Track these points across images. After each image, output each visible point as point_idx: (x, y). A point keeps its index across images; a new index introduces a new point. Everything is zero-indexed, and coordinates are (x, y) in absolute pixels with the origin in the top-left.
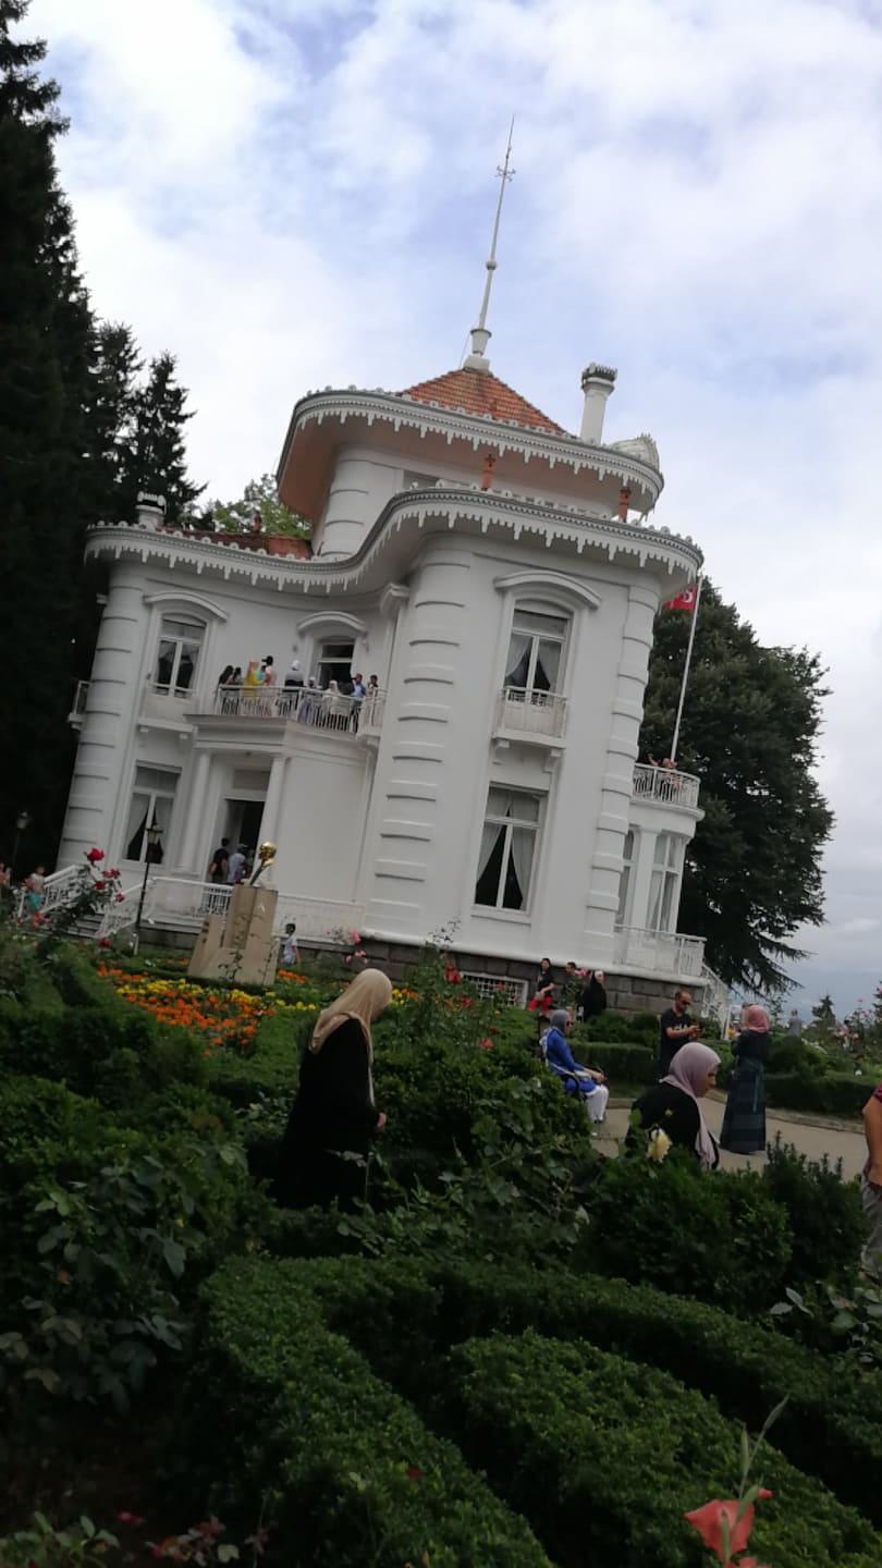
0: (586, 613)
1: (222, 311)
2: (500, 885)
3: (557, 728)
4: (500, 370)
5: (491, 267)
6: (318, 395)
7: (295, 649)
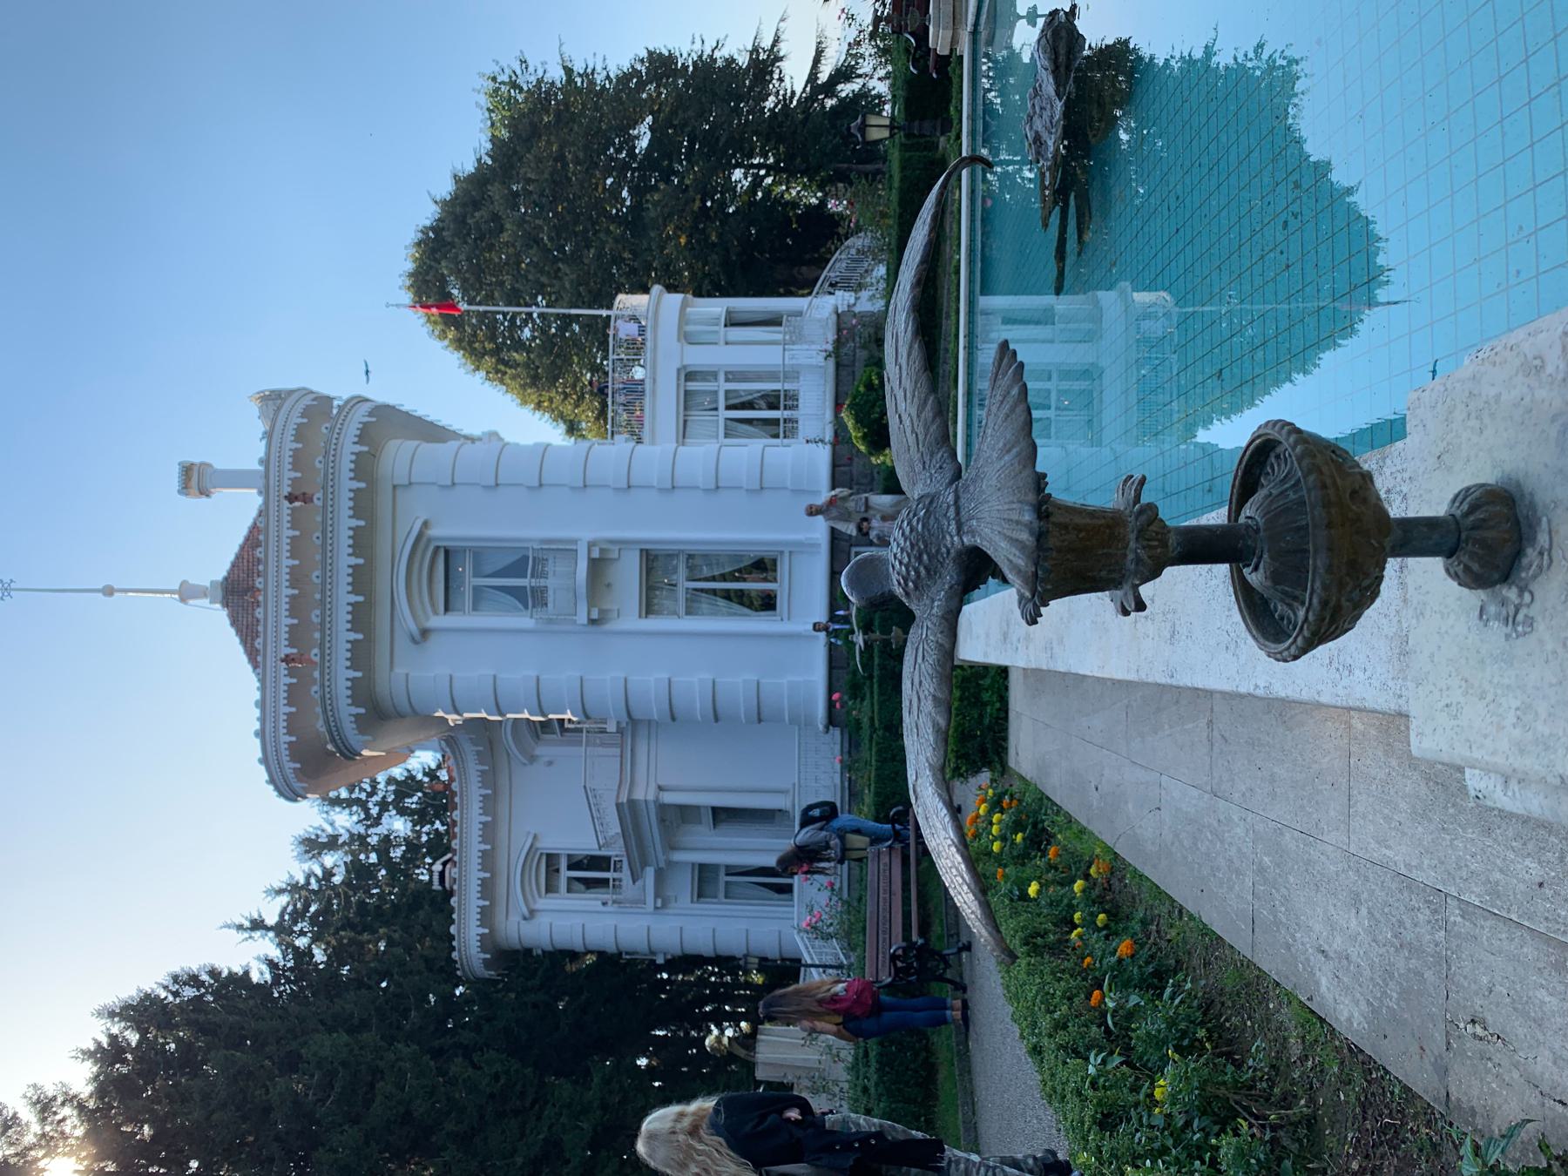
0: (433, 532)
1: (214, 872)
2: (748, 582)
3: (567, 551)
4: (220, 571)
5: (109, 591)
6: (277, 788)
7: (550, 763)
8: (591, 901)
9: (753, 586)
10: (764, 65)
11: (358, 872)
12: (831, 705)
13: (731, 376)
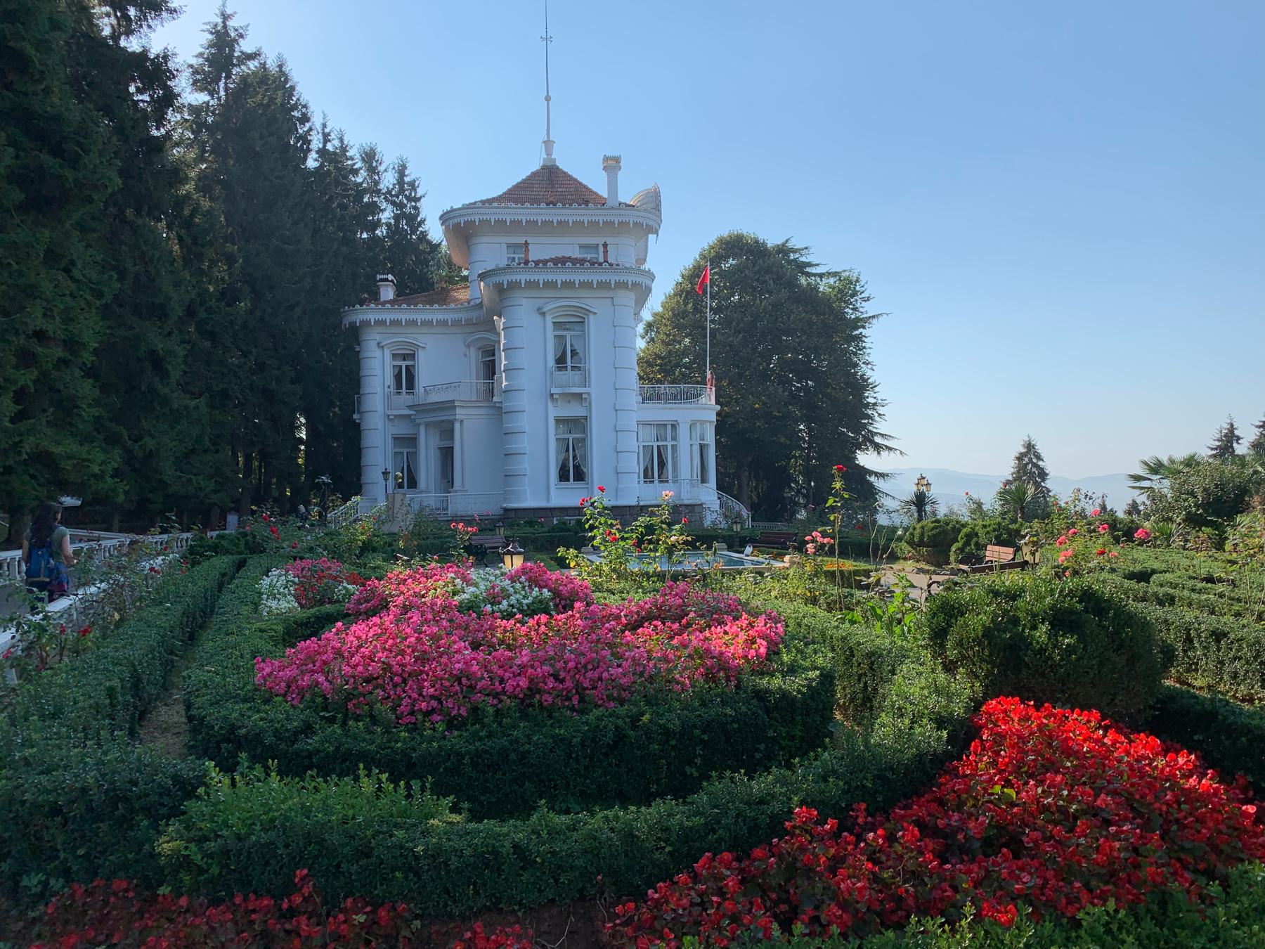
0: (591, 316)
2: (572, 471)
3: (584, 384)
4: (562, 165)
5: (548, 99)
6: (448, 212)
8: (390, 380)
10: (870, 441)
11: (360, 193)
12: (516, 510)
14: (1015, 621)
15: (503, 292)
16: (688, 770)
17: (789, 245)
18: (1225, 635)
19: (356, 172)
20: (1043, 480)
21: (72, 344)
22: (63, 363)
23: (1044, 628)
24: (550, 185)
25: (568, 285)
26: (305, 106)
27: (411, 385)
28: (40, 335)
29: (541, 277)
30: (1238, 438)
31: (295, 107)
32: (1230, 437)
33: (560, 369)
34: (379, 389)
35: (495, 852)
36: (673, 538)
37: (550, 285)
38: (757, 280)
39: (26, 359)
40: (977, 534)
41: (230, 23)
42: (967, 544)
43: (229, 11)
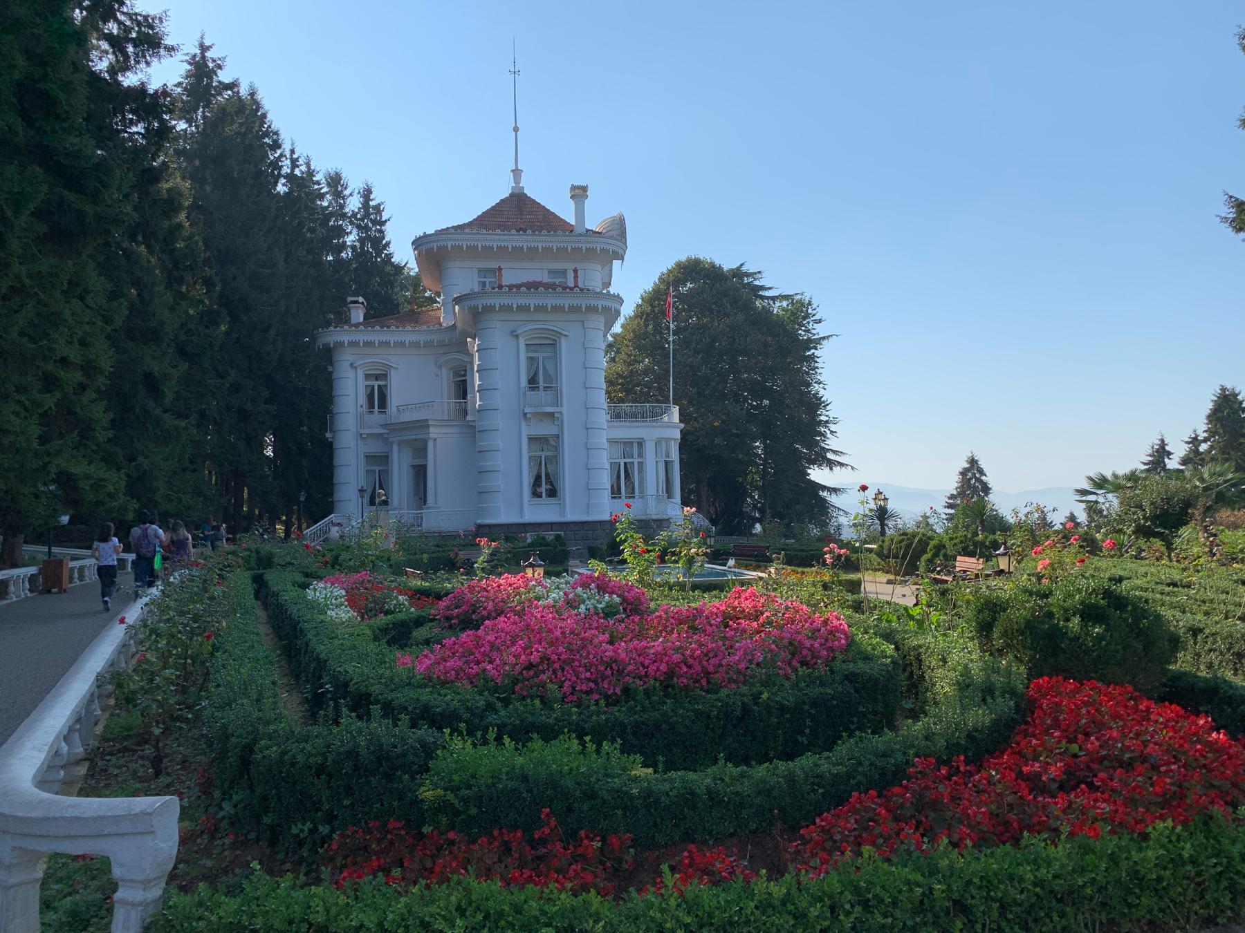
3: (557, 402)
4: (529, 192)
5: (516, 130)
6: (420, 238)
8: (363, 400)
9: (543, 488)
10: (821, 458)
11: (327, 217)
13: (641, 464)
14: (1050, 615)
15: (477, 317)
16: (800, 738)
17: (744, 269)
18: (1201, 630)
19: (322, 196)
20: (987, 494)
21: (89, 369)
22: (82, 387)
23: (1076, 620)
24: (518, 212)
25: (541, 309)
26: (276, 133)
27: (383, 404)
28: (64, 361)
29: (515, 301)
30: (1169, 454)
31: (267, 134)
32: (1161, 452)
33: (533, 389)
34: (352, 410)
35: (693, 793)
36: (693, 551)
37: (524, 309)
38: (715, 303)
39: (50, 383)
40: (944, 546)
41: (208, 54)
42: (936, 555)
43: (207, 43)
